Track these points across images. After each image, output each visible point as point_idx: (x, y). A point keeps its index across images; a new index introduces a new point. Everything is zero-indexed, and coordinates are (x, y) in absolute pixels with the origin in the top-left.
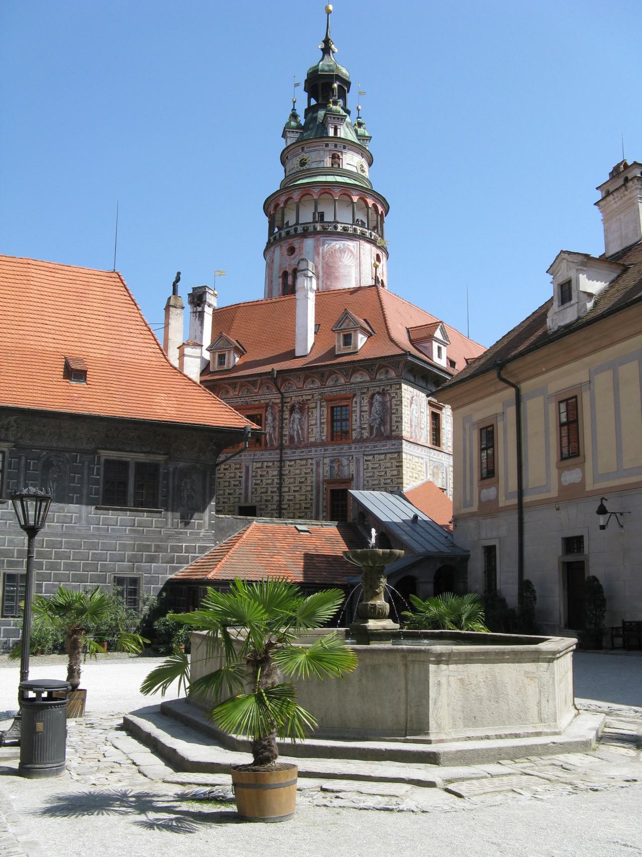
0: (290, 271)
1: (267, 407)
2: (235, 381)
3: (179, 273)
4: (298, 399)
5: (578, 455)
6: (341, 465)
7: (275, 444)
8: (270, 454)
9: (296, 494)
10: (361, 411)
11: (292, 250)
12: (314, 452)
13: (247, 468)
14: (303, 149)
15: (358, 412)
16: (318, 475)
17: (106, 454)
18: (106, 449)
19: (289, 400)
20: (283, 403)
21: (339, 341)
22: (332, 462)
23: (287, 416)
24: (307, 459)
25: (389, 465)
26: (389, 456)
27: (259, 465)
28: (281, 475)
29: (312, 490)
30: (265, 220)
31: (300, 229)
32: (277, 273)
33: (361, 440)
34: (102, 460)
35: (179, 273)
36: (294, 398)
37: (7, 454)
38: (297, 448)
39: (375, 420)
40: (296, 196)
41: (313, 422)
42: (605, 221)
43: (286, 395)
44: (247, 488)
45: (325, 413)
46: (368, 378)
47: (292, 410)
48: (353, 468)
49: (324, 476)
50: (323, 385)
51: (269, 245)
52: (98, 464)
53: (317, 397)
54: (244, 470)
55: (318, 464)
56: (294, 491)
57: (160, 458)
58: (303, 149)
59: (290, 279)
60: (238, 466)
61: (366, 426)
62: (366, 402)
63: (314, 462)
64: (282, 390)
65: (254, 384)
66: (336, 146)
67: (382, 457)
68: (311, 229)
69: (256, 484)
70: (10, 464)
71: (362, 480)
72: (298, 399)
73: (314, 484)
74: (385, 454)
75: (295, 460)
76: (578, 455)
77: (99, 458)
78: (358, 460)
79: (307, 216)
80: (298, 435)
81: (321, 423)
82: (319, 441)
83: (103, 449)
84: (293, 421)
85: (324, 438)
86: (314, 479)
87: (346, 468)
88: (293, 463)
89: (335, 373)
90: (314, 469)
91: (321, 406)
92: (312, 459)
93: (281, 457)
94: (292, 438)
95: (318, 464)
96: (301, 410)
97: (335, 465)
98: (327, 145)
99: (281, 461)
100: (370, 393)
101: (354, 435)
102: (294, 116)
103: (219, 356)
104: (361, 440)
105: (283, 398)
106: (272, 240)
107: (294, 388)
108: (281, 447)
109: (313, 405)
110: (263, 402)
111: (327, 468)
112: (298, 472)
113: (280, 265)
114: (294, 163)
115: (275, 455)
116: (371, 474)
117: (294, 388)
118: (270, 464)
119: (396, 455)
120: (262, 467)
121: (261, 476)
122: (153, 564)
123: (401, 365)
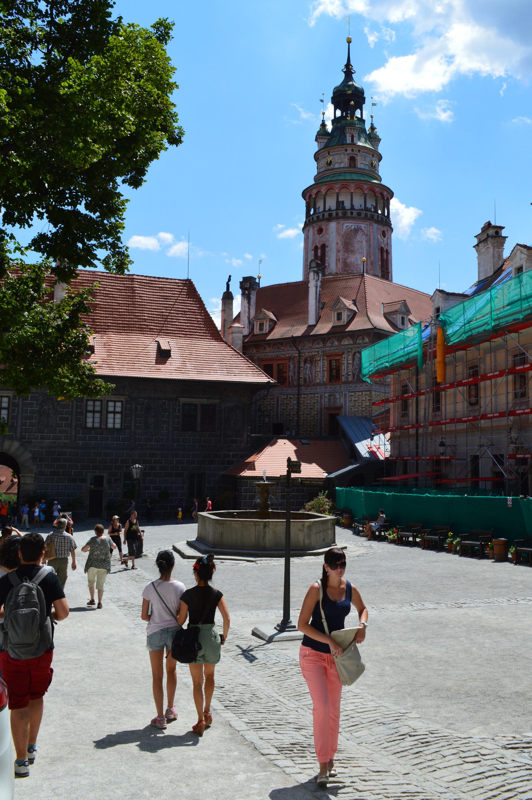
0: (319, 246)
1: (290, 359)
2: (269, 342)
3: (230, 276)
4: (309, 354)
5: (439, 410)
6: (335, 398)
7: (295, 383)
8: (292, 390)
9: (308, 416)
10: (348, 364)
11: (320, 231)
12: (319, 389)
13: (278, 398)
14: (329, 153)
15: (346, 364)
16: (321, 404)
17: (183, 400)
18: (183, 397)
19: (303, 355)
20: (300, 356)
21: (334, 317)
22: (330, 396)
23: (302, 366)
24: (314, 394)
25: (364, 399)
26: (364, 393)
27: (285, 397)
28: (298, 403)
29: (317, 414)
30: (303, 203)
31: (326, 215)
32: (311, 247)
33: (347, 382)
34: (181, 403)
35: (230, 276)
36: (307, 354)
37: (124, 403)
38: (308, 386)
39: (356, 369)
40: (323, 190)
41: (318, 370)
42: (479, 258)
43: (302, 351)
44: (277, 412)
45: (326, 364)
46: (352, 342)
47: (305, 362)
48: (342, 400)
49: (325, 405)
50: (325, 345)
51: (306, 225)
52: (179, 406)
53: (320, 353)
54: (276, 400)
55: (321, 397)
56: (307, 414)
57: (216, 401)
58: (329, 153)
59: (319, 252)
60: (272, 397)
61: (350, 373)
62: (350, 357)
63: (319, 395)
64: (299, 348)
65: (282, 344)
66: (353, 150)
67: (360, 393)
68: (334, 214)
69: (283, 409)
70: (126, 408)
71: (348, 409)
72: (309, 354)
73: (319, 410)
74: (362, 391)
75: (307, 394)
76: (439, 410)
77: (179, 403)
78: (345, 395)
79: (331, 203)
80: (309, 377)
81: (323, 371)
82: (322, 382)
83: (181, 397)
84: (306, 368)
85: (325, 380)
86: (319, 407)
87: (338, 400)
88: (306, 396)
89: (331, 338)
90: (319, 400)
91: (323, 360)
92: (318, 393)
93: (299, 392)
94: (305, 379)
95: (321, 397)
96: (311, 362)
97: (332, 398)
98: (346, 150)
99: (299, 394)
100: (353, 352)
101: (343, 379)
102: (323, 125)
103: (260, 324)
104: (347, 382)
105: (300, 353)
106: (307, 222)
107: (307, 347)
108: (299, 386)
109: (319, 359)
110: (287, 355)
111: (327, 400)
112: (309, 401)
113: (313, 241)
114: (323, 162)
115: (295, 391)
116: (353, 404)
117: (307, 347)
118: (292, 396)
119: (368, 393)
120: (287, 398)
121: (287, 404)
122: (213, 466)
123: (372, 335)
